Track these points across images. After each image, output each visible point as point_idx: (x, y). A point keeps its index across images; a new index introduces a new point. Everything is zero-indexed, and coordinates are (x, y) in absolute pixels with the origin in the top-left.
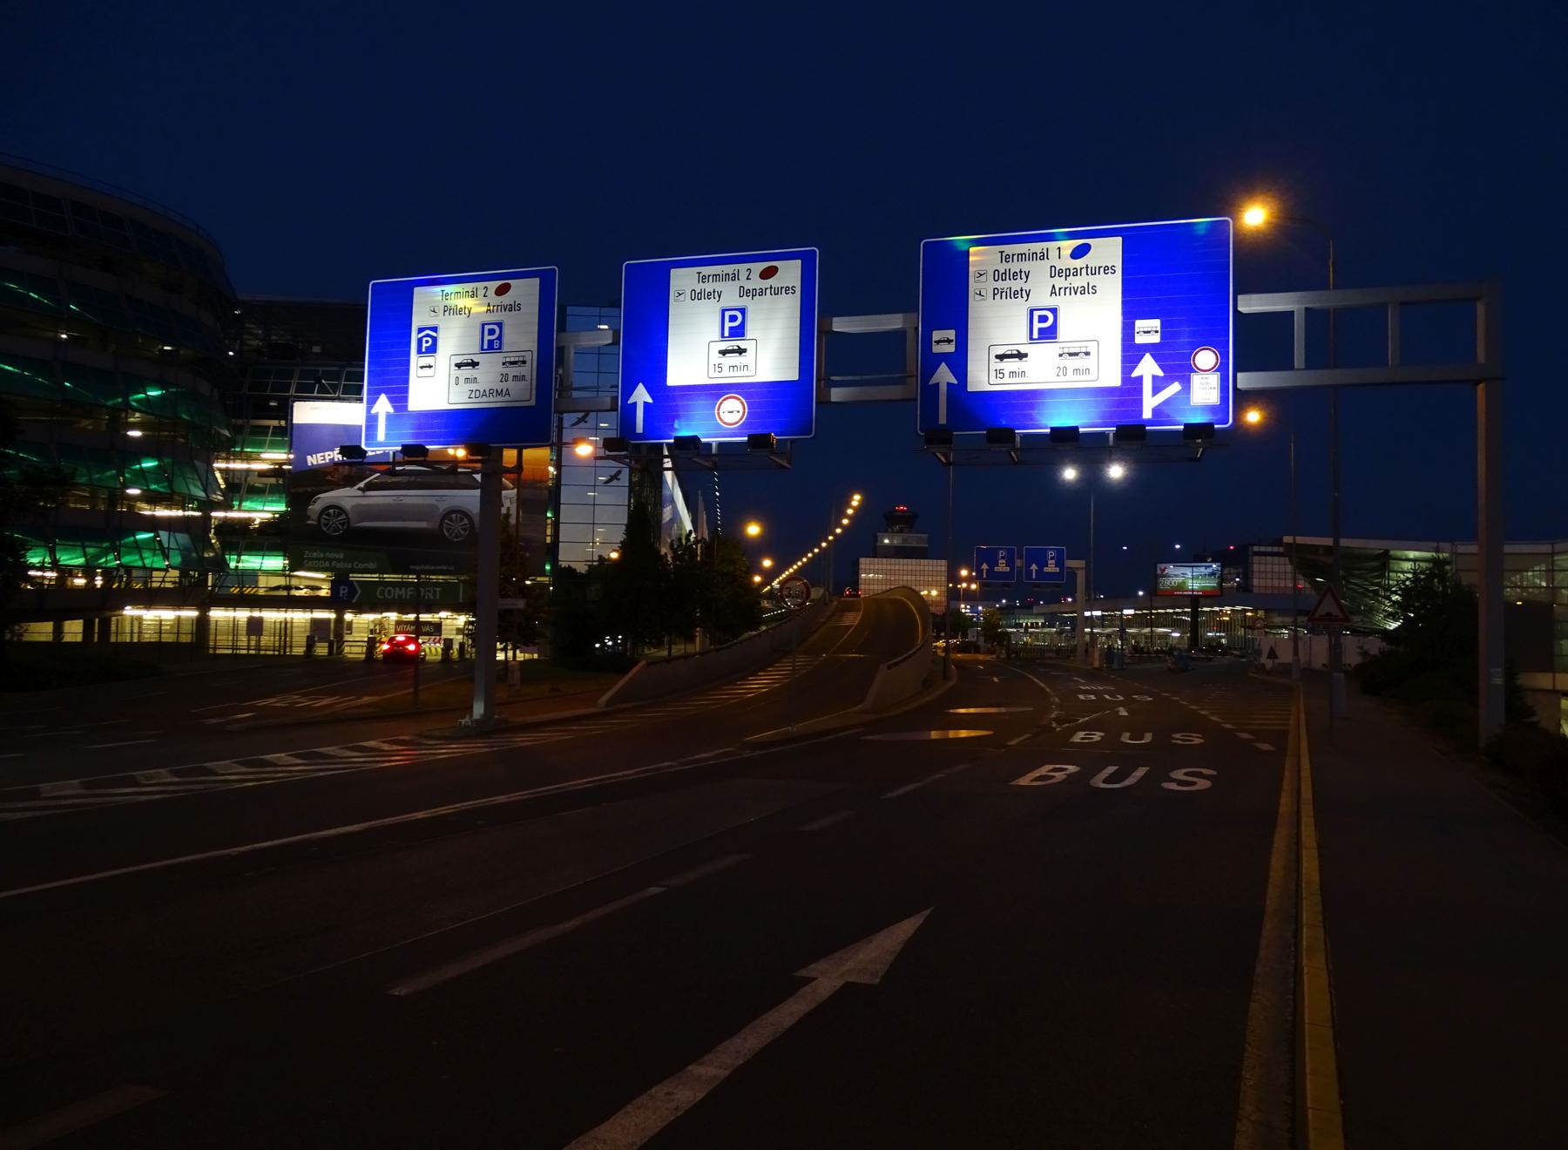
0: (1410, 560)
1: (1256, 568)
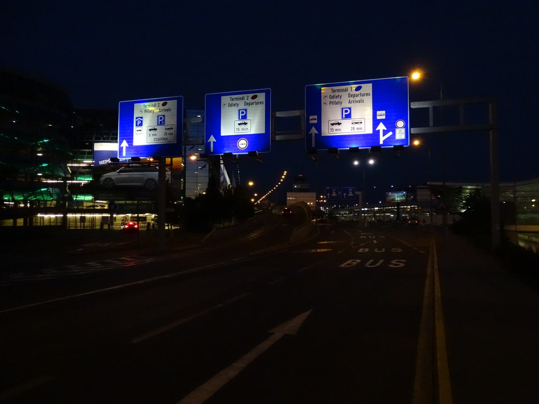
0: (469, 188)
1: (418, 193)
